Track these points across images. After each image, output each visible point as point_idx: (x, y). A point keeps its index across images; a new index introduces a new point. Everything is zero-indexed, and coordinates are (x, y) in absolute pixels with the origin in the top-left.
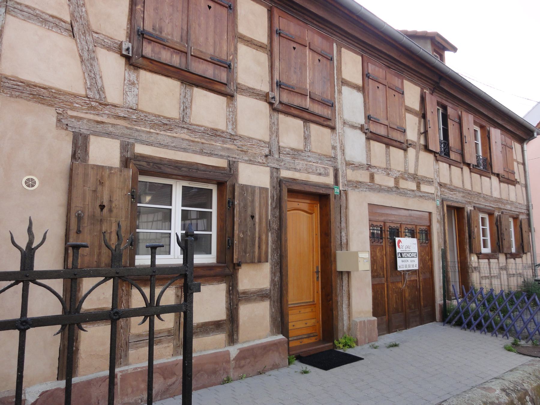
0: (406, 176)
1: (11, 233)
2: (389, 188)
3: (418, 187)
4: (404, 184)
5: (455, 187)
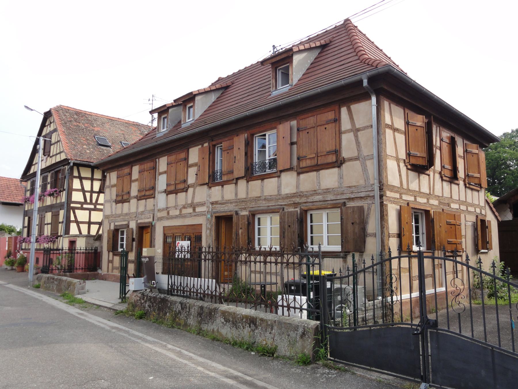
0: (186, 206)
1: (32, 110)
2: (176, 216)
3: (194, 210)
4: (184, 211)
5: (226, 200)
